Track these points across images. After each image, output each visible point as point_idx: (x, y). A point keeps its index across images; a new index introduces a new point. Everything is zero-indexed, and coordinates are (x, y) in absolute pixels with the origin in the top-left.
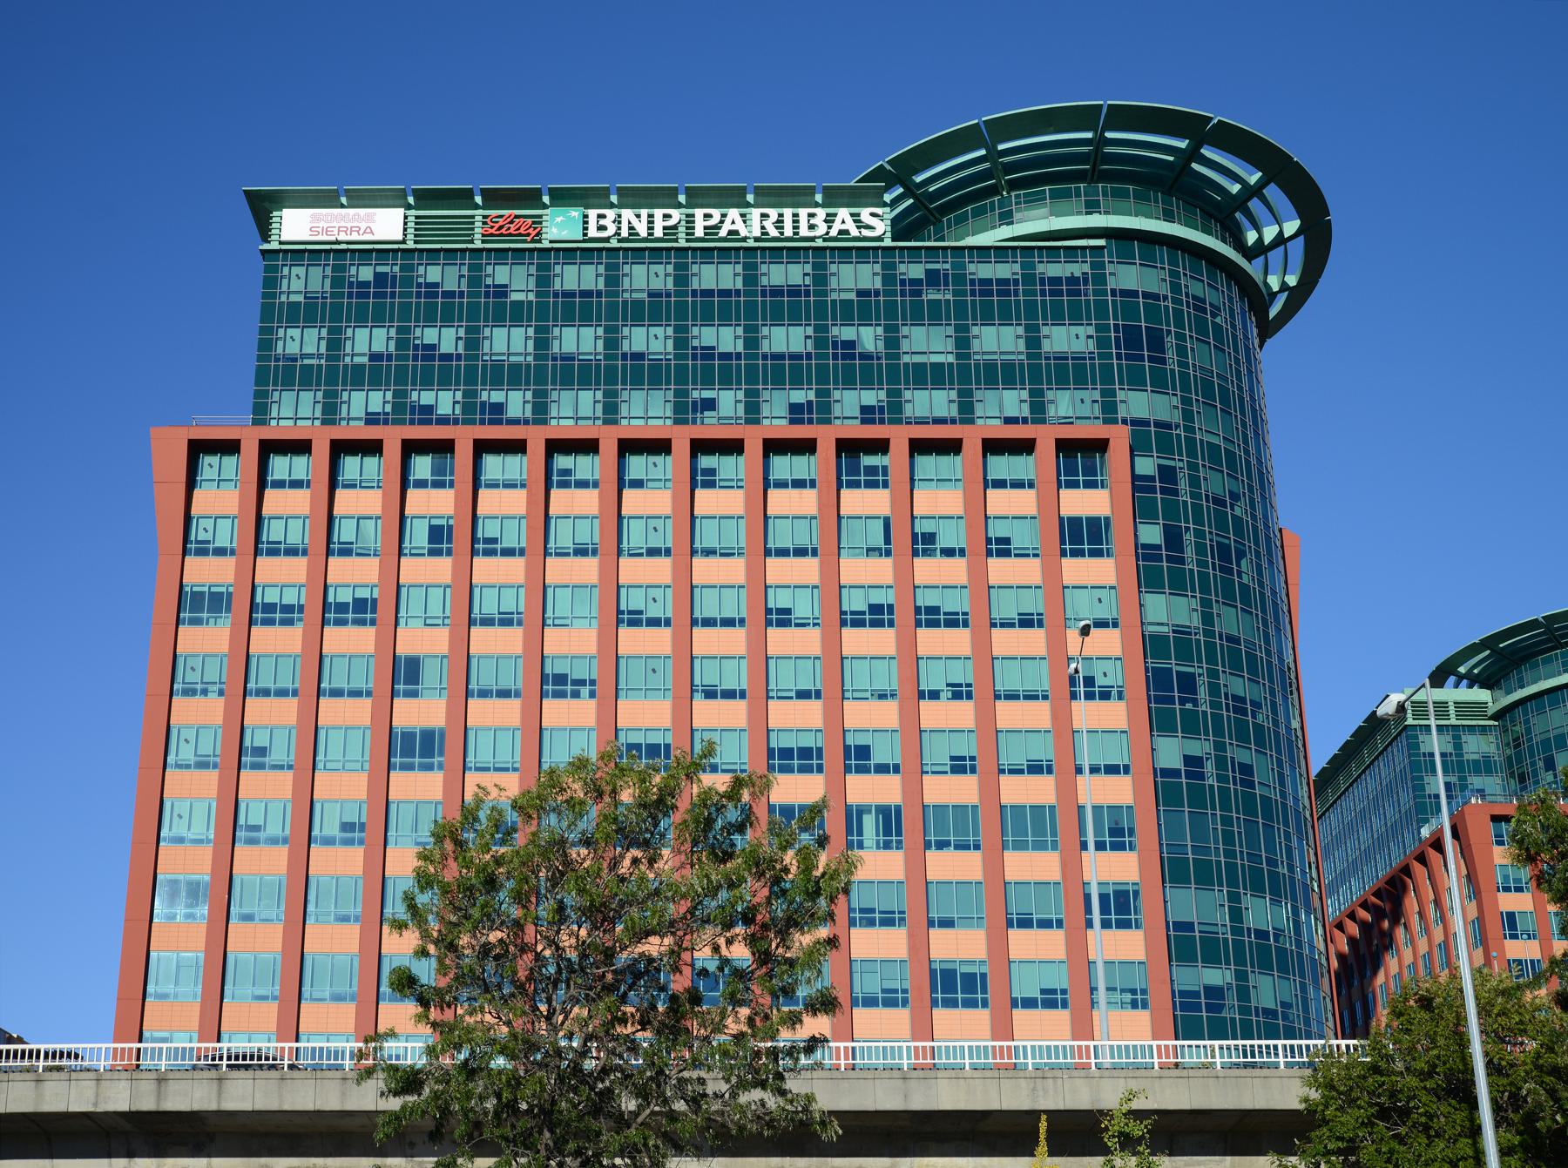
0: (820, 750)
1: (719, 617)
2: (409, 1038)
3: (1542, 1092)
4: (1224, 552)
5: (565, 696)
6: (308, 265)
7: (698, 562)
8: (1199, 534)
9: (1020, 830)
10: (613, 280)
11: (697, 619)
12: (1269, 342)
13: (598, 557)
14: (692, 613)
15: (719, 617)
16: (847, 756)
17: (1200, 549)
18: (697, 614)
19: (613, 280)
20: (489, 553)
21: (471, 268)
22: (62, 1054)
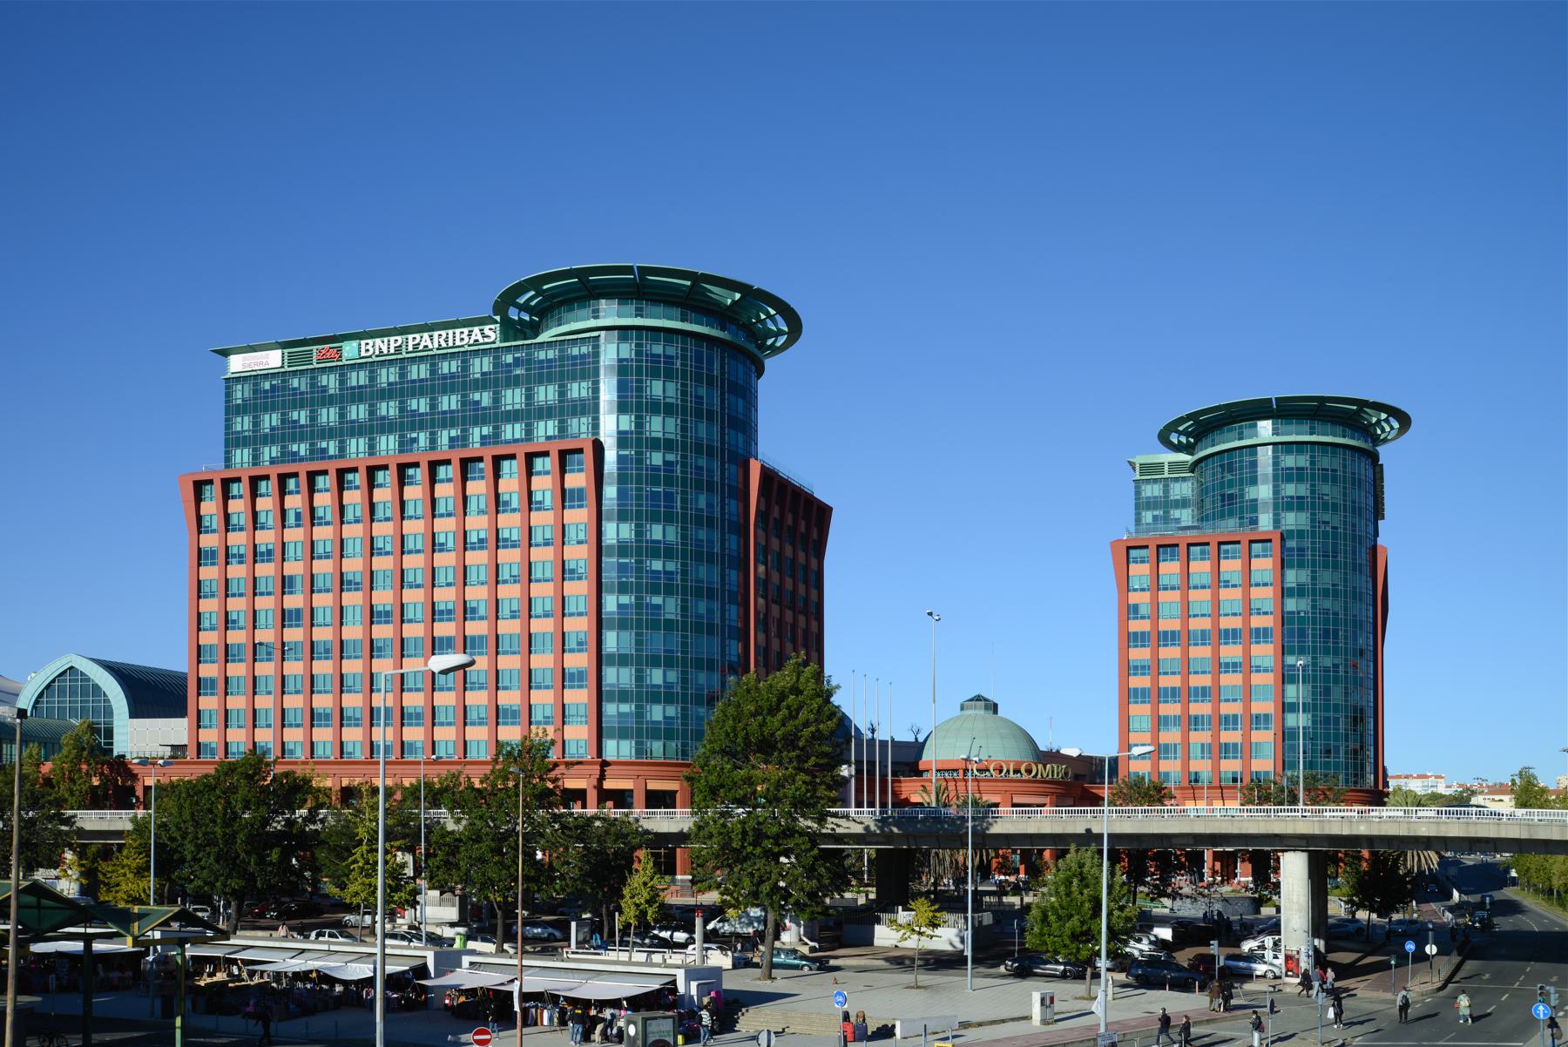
17: (1314, 636)
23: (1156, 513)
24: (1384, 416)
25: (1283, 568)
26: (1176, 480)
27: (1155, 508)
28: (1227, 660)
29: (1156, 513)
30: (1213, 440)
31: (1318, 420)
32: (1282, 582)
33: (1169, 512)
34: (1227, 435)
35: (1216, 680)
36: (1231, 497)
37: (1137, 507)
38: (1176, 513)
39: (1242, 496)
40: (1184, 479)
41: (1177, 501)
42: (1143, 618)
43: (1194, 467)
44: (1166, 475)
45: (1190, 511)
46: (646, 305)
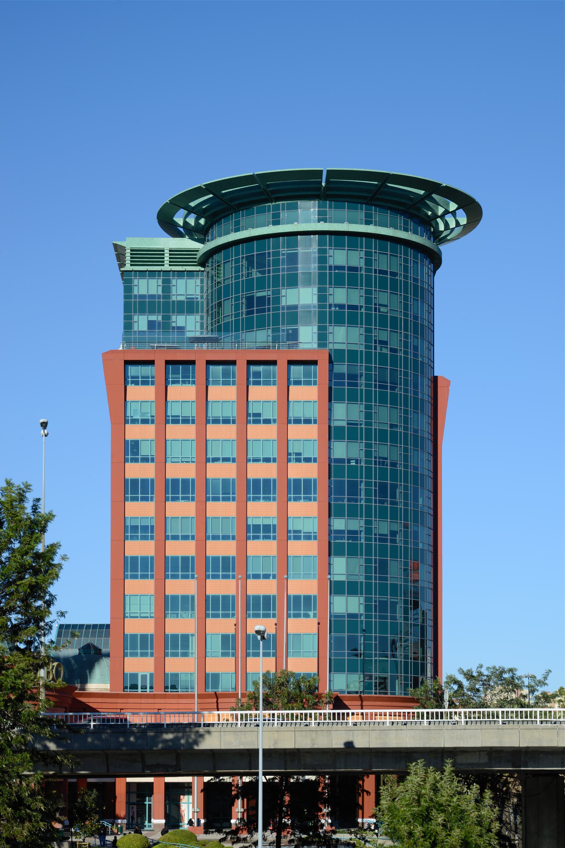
0: (152, 527)
1: (221, 457)
2: (365, 703)
3: (58, 680)
4: (383, 489)
5: (219, 500)
6: (334, 249)
7: (170, 427)
8: (368, 484)
9: (175, 568)
10: (167, 288)
11: (209, 458)
12: (438, 272)
13: (276, 424)
14: (206, 455)
15: (221, 457)
16: (248, 531)
17: (368, 492)
18: (209, 456)
19: (167, 288)
20: (256, 422)
21: (164, 281)
22: (395, 715)
23: (153, 318)
24: (453, 206)
25: (330, 400)
26: (180, 274)
27: (152, 311)
28: (256, 522)
29: (153, 318)
30: (237, 223)
31: (376, 206)
32: (330, 419)
33: (169, 318)
34: (256, 217)
35: (242, 549)
36: (262, 300)
37: (127, 307)
38: (179, 320)
39: (277, 300)
40: (191, 274)
41: (180, 303)
42: (145, 460)
43: (204, 260)
44: (167, 267)
45: (198, 318)
46: (375, 211)
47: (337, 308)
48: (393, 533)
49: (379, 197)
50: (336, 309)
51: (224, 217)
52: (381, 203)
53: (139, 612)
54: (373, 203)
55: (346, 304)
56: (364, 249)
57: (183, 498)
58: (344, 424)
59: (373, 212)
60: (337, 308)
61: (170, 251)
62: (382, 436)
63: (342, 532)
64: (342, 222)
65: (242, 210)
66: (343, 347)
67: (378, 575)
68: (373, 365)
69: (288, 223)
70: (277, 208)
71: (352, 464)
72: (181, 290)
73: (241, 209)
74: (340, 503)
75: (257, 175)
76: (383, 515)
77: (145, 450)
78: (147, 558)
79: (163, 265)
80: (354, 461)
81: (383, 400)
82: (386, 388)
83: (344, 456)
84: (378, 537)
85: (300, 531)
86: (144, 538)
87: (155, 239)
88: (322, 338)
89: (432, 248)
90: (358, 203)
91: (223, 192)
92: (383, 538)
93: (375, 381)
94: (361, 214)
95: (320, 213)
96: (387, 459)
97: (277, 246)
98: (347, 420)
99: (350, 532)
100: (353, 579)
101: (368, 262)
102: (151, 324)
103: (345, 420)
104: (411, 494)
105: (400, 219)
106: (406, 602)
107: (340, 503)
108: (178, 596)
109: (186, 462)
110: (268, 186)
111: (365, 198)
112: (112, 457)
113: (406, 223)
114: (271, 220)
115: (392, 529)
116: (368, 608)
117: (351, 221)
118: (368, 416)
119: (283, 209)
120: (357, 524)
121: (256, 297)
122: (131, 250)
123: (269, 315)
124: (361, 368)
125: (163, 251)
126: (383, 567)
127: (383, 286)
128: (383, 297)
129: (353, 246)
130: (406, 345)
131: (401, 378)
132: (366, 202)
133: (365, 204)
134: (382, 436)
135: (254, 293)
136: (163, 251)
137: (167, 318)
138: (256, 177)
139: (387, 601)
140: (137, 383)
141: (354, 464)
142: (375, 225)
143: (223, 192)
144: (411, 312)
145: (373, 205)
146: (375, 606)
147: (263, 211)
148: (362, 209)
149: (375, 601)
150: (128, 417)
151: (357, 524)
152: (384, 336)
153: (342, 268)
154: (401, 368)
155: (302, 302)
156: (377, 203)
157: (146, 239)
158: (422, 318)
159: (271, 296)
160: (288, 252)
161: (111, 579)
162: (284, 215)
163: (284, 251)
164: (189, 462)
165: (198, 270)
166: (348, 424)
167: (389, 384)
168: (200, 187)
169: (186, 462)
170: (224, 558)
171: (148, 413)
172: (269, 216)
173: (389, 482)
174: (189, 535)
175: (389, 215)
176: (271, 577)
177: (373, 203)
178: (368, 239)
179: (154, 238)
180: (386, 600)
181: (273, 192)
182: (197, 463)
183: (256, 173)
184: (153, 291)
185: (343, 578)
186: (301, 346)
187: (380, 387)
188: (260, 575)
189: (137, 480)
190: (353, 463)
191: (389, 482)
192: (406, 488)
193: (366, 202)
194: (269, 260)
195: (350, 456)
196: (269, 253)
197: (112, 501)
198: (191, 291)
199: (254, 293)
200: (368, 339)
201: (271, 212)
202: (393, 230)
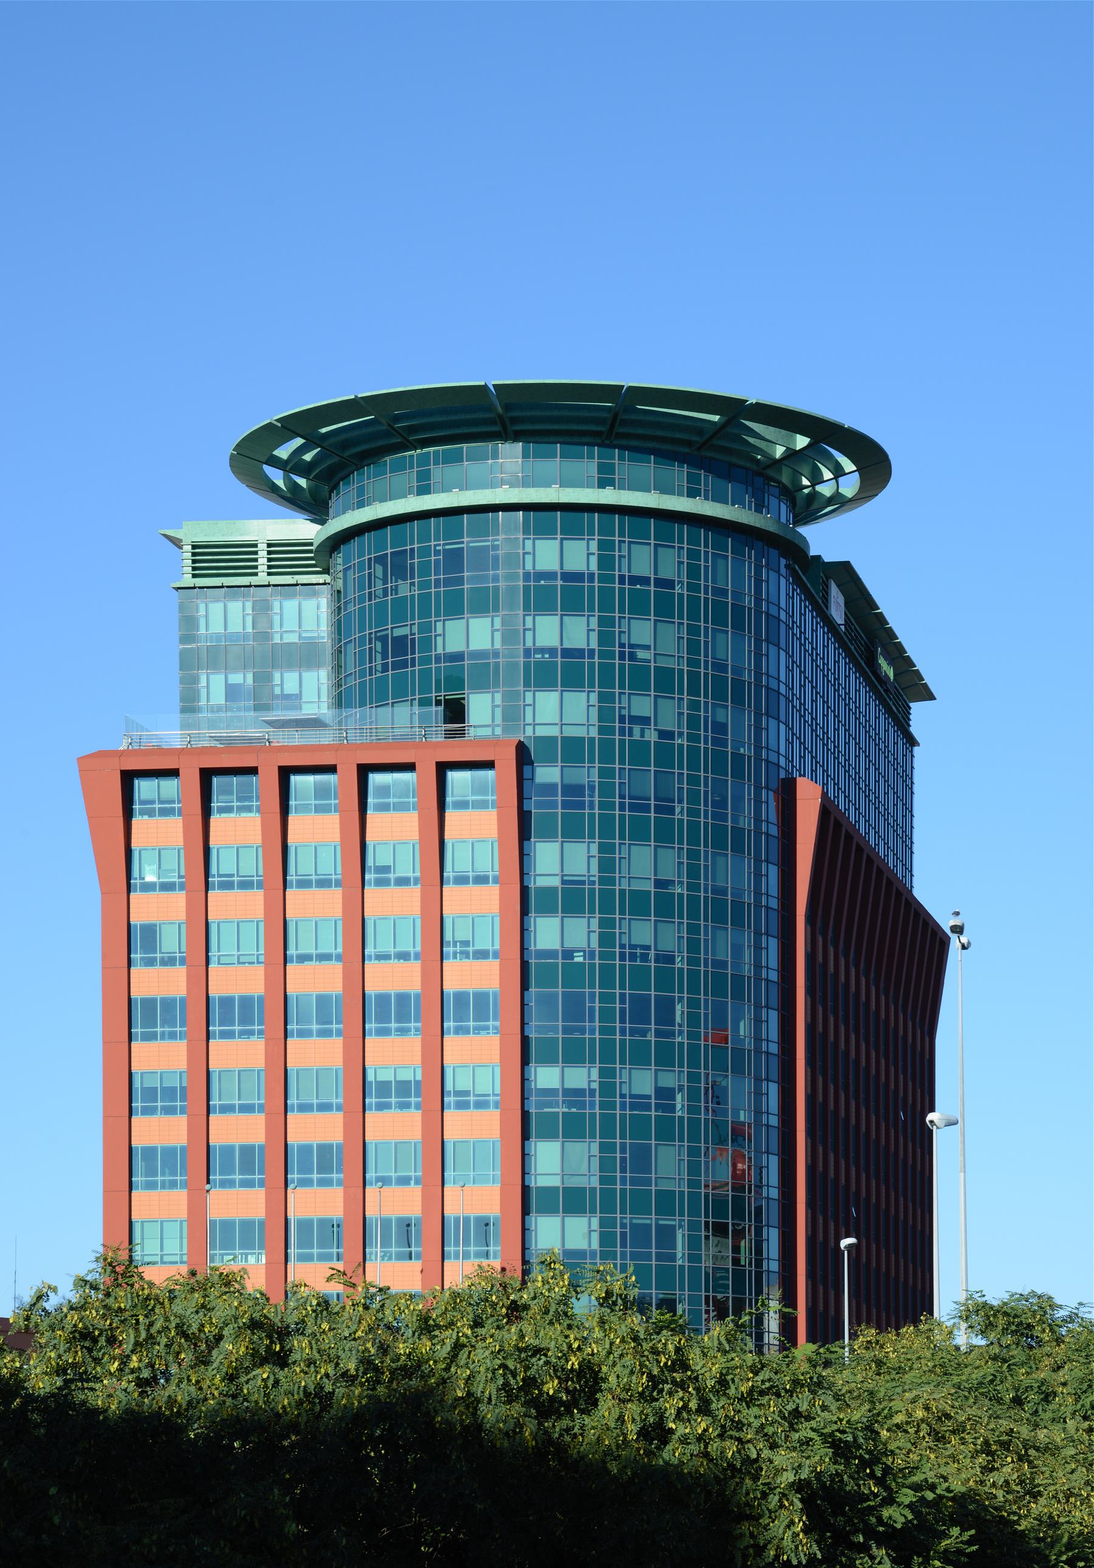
13: (419, 886)
23: (236, 678)
28: (386, 1075)
29: (236, 678)
30: (361, 491)
31: (622, 448)
38: (288, 681)
39: (427, 643)
42: (169, 961)
44: (262, 578)
47: (547, 656)
48: (665, 1094)
49: (622, 430)
50: (543, 657)
51: (342, 479)
52: (634, 443)
53: (159, 1252)
54: (615, 442)
55: (586, 648)
56: (596, 537)
57: (242, 1033)
58: (555, 882)
59: (617, 462)
60: (547, 656)
61: (269, 545)
62: (637, 904)
63: (552, 1092)
64: (547, 485)
65: (368, 465)
66: (554, 731)
67: (628, 1175)
68: (617, 766)
69: (444, 490)
70: (424, 460)
71: (576, 960)
72: (291, 624)
73: (365, 463)
74: (577, 1035)
75: (361, 398)
76: (639, 1057)
77: (171, 941)
78: (252, 1148)
79: (256, 574)
80: (582, 954)
81: (639, 834)
82: (647, 808)
83: (556, 946)
84: (628, 1100)
85: (466, 1093)
86: (169, 1111)
87: (240, 523)
88: (512, 714)
89: (758, 525)
90: (583, 444)
91: (324, 430)
92: (639, 1102)
93: (622, 796)
94: (590, 467)
95: (601, 469)
96: (648, 948)
97: (425, 537)
98: (563, 876)
99: (567, 1092)
100: (574, 1182)
101: (605, 562)
102: (232, 692)
103: (557, 875)
104: (706, 1015)
105: (680, 473)
106: (693, 1226)
107: (577, 1035)
108: (233, 1223)
109: (250, 963)
110: (397, 419)
111: (598, 434)
112: (105, 956)
113: (692, 479)
114: (416, 484)
115: (662, 1083)
116: (606, 1239)
117: (665, 489)
118: (606, 865)
119: (436, 463)
120: (581, 1077)
121: (393, 638)
122: (194, 547)
123: (413, 672)
124: (588, 774)
125: (256, 546)
126: (641, 1160)
127: (638, 607)
128: (642, 631)
129: (571, 532)
130: (693, 722)
131: (681, 789)
132: (599, 441)
133: (599, 445)
134: (637, 904)
135: (387, 629)
136: (256, 546)
137: (263, 679)
138: (363, 403)
139: (651, 1225)
140: (151, 813)
141: (581, 959)
142: (706, 498)
143: (324, 430)
144: (706, 656)
145: (615, 447)
146: (623, 1234)
147: (398, 468)
148: (591, 456)
149: (623, 1226)
150: (136, 879)
151: (581, 1077)
152: (642, 706)
153: (549, 575)
154: (681, 767)
155: (473, 647)
156: (624, 442)
157: (222, 524)
158: (738, 670)
159: (417, 636)
160: (447, 547)
161: (104, 1191)
162: (437, 473)
163: (439, 545)
164: (254, 963)
165: (321, 581)
166: (563, 882)
167: (652, 802)
168: (270, 423)
169: (250, 963)
170: (321, 1147)
171: (173, 871)
172: (410, 477)
173: (653, 993)
174: (235, 1105)
175: (652, 465)
176: (412, 1182)
177: (615, 442)
178: (605, 516)
179: (219, 522)
180: (648, 1222)
181: (412, 430)
182: (267, 964)
183: (360, 395)
184: (235, 627)
185: (555, 1182)
186: (472, 733)
187: (633, 807)
188: (390, 1178)
189: (153, 1001)
190: (579, 958)
191: (653, 993)
192: (693, 1004)
193: (599, 441)
194: (412, 565)
195: (568, 945)
196: (412, 550)
197: (105, 1042)
198: (309, 624)
199: (387, 629)
200: (604, 715)
201: (415, 469)
202: (657, 496)
